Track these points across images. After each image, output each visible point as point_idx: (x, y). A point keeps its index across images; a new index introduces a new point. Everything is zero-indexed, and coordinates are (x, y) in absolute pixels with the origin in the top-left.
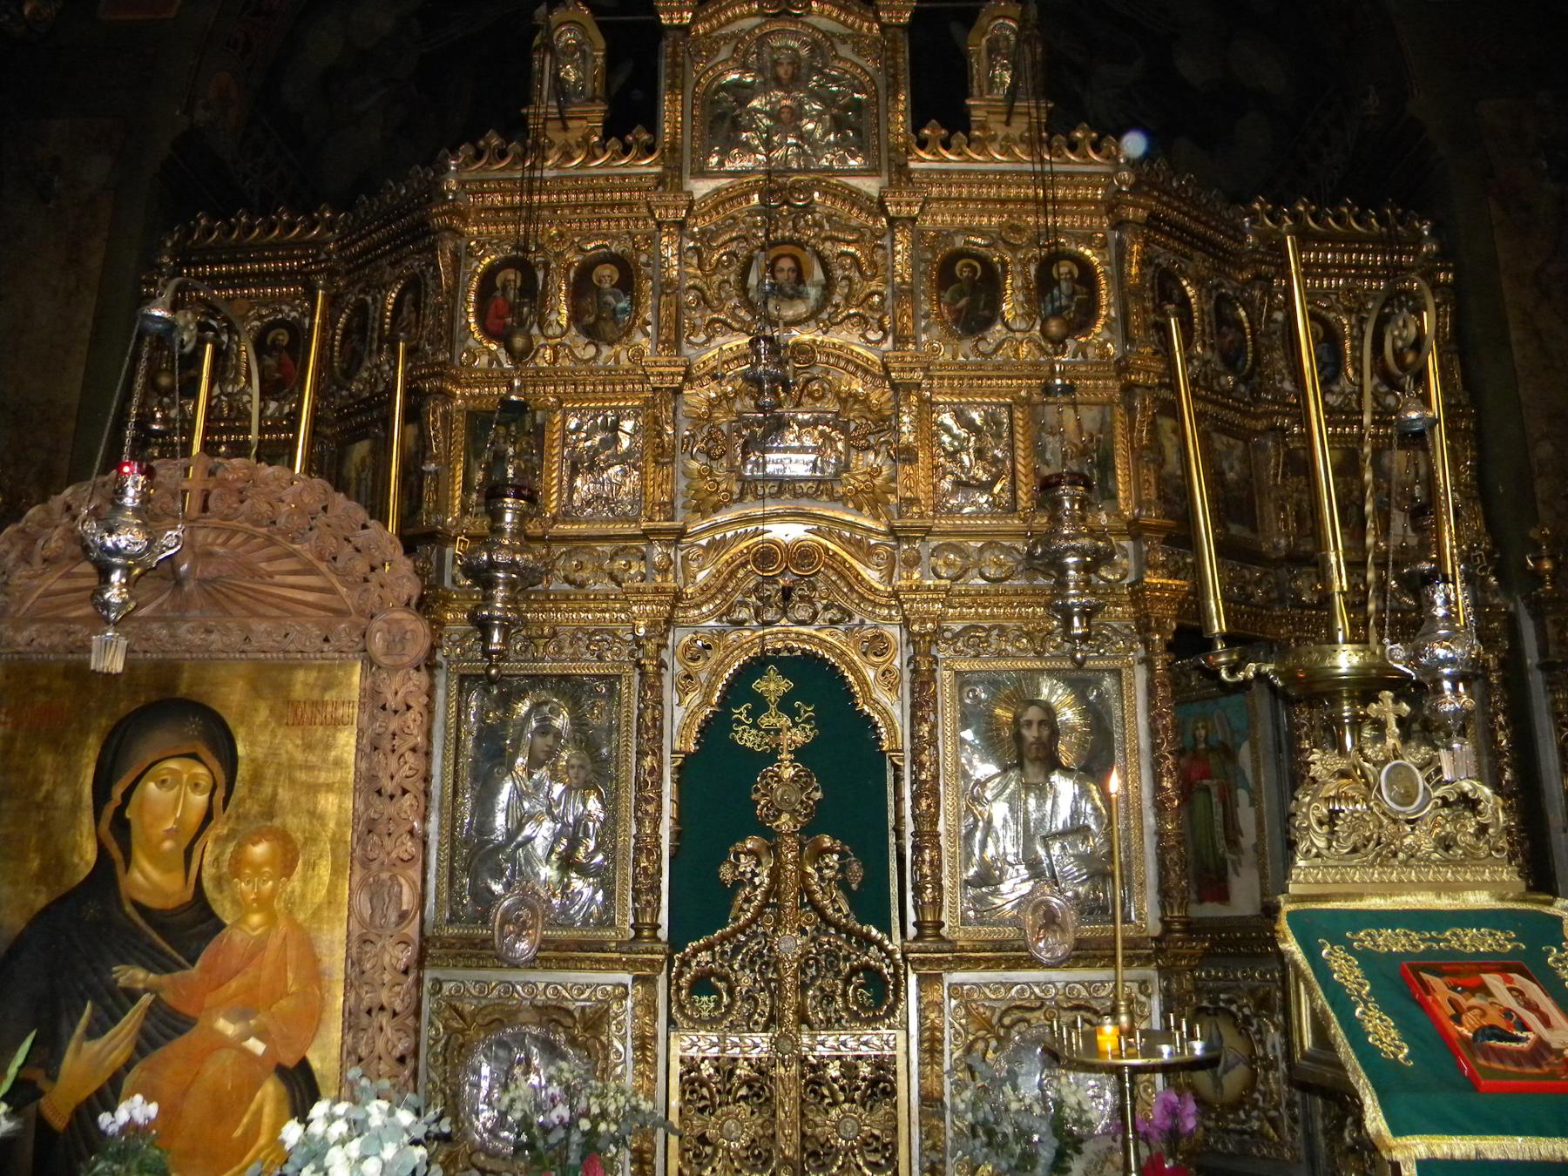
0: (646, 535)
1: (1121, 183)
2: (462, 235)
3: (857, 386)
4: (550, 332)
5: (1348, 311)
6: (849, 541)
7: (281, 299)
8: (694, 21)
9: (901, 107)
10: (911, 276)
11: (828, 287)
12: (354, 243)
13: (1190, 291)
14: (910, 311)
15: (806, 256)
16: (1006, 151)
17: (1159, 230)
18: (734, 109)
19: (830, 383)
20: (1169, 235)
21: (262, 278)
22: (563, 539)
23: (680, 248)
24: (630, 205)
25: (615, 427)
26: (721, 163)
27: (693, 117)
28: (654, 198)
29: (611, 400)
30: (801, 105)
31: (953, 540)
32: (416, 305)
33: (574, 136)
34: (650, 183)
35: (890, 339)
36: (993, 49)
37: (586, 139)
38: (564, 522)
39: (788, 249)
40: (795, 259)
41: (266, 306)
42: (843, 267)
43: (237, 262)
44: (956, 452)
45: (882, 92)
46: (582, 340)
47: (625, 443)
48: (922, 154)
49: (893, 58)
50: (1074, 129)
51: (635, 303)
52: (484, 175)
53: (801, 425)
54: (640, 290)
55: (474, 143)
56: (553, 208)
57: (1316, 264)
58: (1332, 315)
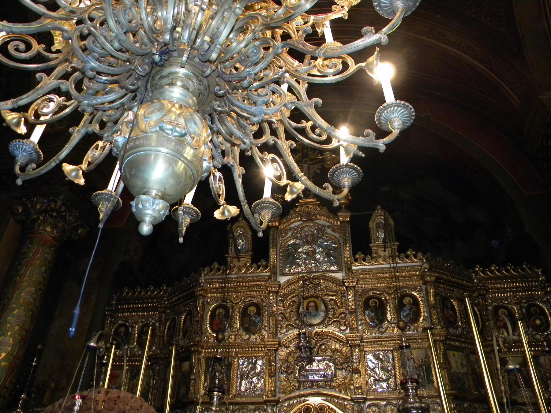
0: (265, 402)
1: (425, 268)
2: (205, 297)
3: (337, 346)
4: (234, 330)
5: (516, 304)
6: (337, 403)
7: (149, 316)
8: (279, 224)
9: (348, 249)
10: (355, 306)
11: (327, 311)
12: (172, 298)
13: (455, 303)
14: (355, 319)
15: (318, 301)
16: (384, 260)
17: (440, 283)
18: (294, 252)
19: (329, 345)
20: (444, 284)
21: (143, 309)
22: (237, 404)
23: (277, 299)
24: (260, 286)
25: (256, 363)
26: (289, 271)
27: (280, 255)
28: (267, 283)
29: (254, 354)
30: (315, 250)
31: (375, 402)
32: (191, 320)
33: (242, 263)
34: (266, 278)
35: (348, 329)
36: (378, 227)
37: (245, 264)
38: (238, 398)
39: (312, 299)
40: (315, 302)
41: (144, 318)
42: (331, 305)
43: (136, 304)
44: (374, 368)
45: (342, 244)
46: (244, 333)
47: (259, 368)
48: (356, 264)
49: (345, 233)
50: (407, 251)
51: (262, 320)
52: (213, 277)
53: (319, 361)
54: (263, 315)
55: (210, 266)
56: (235, 287)
57: (501, 288)
58: (510, 306)
